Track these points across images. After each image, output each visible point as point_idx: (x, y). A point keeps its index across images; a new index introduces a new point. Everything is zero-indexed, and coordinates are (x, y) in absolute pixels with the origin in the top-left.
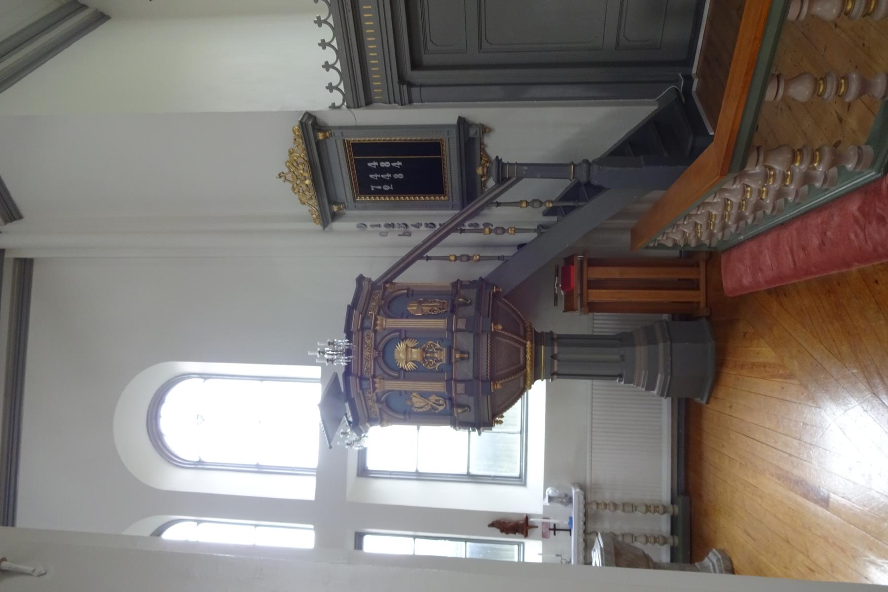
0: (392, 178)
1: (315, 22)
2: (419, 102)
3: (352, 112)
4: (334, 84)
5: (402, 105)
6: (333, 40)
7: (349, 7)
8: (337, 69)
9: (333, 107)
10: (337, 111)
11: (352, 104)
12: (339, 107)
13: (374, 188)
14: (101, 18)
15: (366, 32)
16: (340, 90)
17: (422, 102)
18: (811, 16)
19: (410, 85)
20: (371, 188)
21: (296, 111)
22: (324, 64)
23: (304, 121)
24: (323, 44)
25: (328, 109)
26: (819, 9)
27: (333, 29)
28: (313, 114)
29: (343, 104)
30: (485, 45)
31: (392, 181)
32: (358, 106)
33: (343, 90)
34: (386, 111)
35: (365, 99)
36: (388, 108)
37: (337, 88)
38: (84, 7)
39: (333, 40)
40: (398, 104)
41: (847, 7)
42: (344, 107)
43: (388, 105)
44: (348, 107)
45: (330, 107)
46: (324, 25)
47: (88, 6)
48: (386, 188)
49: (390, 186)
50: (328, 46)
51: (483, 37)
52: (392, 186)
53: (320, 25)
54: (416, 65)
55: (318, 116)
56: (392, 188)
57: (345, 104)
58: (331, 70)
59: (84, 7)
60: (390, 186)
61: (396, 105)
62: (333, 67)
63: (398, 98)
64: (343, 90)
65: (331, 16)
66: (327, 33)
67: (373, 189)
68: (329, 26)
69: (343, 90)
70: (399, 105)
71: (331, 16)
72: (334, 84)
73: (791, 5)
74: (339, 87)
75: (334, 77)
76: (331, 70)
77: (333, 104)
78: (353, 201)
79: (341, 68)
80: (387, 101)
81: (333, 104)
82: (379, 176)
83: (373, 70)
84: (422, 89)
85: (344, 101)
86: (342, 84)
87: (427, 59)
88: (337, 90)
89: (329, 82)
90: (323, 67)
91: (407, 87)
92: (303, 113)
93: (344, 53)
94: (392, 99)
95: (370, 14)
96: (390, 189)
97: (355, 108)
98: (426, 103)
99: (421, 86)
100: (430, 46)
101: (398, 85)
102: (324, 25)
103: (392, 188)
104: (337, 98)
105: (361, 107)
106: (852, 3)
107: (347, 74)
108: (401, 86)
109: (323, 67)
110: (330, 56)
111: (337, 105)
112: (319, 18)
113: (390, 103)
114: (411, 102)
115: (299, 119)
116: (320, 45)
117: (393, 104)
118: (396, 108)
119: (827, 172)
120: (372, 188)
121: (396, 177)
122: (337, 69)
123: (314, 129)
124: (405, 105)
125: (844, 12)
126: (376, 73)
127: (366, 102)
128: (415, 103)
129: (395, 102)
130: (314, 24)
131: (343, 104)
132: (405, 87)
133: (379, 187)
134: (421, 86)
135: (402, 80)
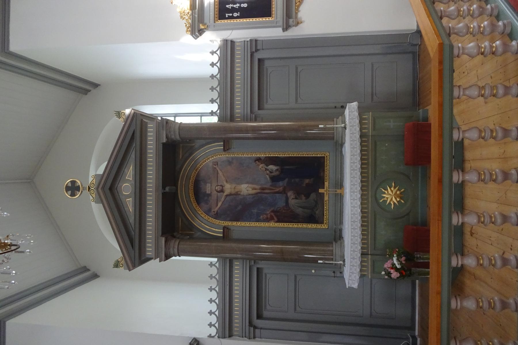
0: (240, 7)
1: (209, 289)
2: (259, 338)
3: (220, 341)
4: (213, 323)
5: (249, 339)
6: (216, 275)
7: (228, 283)
8: (216, 315)
9: (210, 336)
10: (212, 339)
11: (221, 336)
12: (213, 337)
13: (228, 16)
14: (95, 276)
15: (236, 61)
16: (215, 327)
17: (261, 338)
18: (462, 308)
19: (255, 328)
20: (226, 15)
21: (189, 337)
22: (209, 311)
23: (192, 343)
24: (211, 301)
25: (207, 337)
26: (467, 93)
27: (218, 293)
28: (198, 340)
29: (216, 335)
30: (299, 100)
31: (240, 9)
32: (224, 337)
33: (217, 327)
34: (240, 341)
35: (229, 334)
36: (240, 340)
37: (214, 325)
38: (88, 270)
39: (216, 298)
40: (247, 338)
41: (480, 304)
42: (216, 337)
43: (241, 338)
44: (219, 337)
45: (208, 336)
46: (213, 279)
47: (91, 270)
48: (235, 15)
49: (238, 14)
50: (213, 326)
51: (297, 304)
52: (239, 13)
53: (211, 291)
54: (259, 316)
55: (201, 341)
56: (239, 15)
57: (217, 335)
58: (213, 267)
59: (88, 270)
60: (238, 14)
61: (246, 338)
62: (214, 313)
63: (247, 335)
64: (217, 327)
65: (218, 287)
66: (214, 295)
67: (227, 16)
68: (216, 268)
69: (217, 327)
70: (247, 339)
71: (218, 287)
72: (213, 323)
73: (454, 108)
74: (215, 325)
75: (213, 319)
76: (213, 267)
77: (210, 335)
78: (213, 22)
79: (218, 290)
80: (241, 336)
81: (210, 335)
82: (232, 6)
83: (235, 317)
84: (262, 330)
85: (216, 334)
86: (217, 299)
87: (266, 314)
88: (214, 326)
89: (210, 333)
90: (209, 313)
91: (253, 328)
92: (193, 338)
93: (222, 307)
94: (244, 335)
95: (238, 291)
96: (238, 16)
97: (222, 338)
98: (263, 339)
99: (261, 329)
100: (268, 307)
101: (248, 326)
102: (213, 279)
103: (239, 15)
104: (213, 331)
105: (226, 338)
106: (483, 218)
107: (221, 319)
108: (250, 327)
109: (209, 313)
110: (214, 307)
111: (212, 335)
112: (211, 287)
113: (242, 337)
114: (254, 338)
115: (190, 342)
116: (209, 301)
117: (245, 338)
118: (246, 341)
119: (489, 180)
120: (227, 15)
121: (242, 6)
122: (216, 315)
123: (198, 21)
124: (251, 339)
125: (479, 264)
126: (237, 319)
127: (229, 336)
128: (257, 339)
129: (245, 337)
130: (208, 326)
131: (216, 335)
132: (252, 328)
133: (231, 15)
134: (261, 329)
135: (251, 324)
